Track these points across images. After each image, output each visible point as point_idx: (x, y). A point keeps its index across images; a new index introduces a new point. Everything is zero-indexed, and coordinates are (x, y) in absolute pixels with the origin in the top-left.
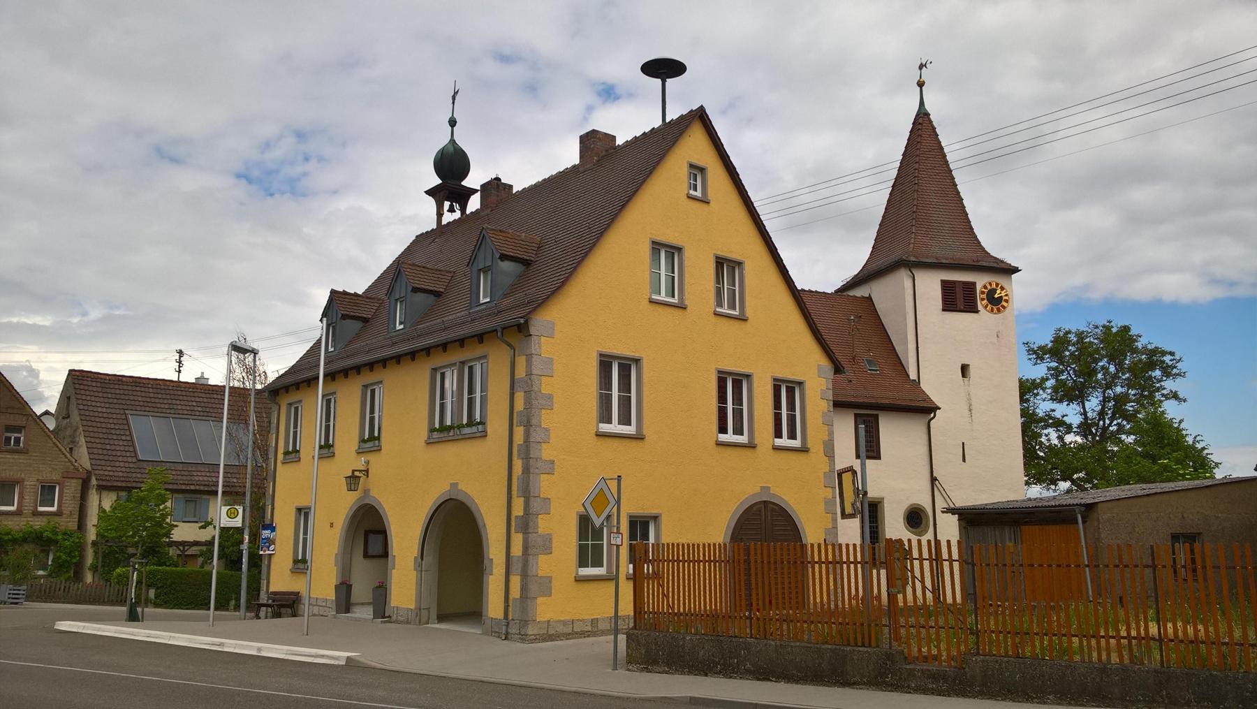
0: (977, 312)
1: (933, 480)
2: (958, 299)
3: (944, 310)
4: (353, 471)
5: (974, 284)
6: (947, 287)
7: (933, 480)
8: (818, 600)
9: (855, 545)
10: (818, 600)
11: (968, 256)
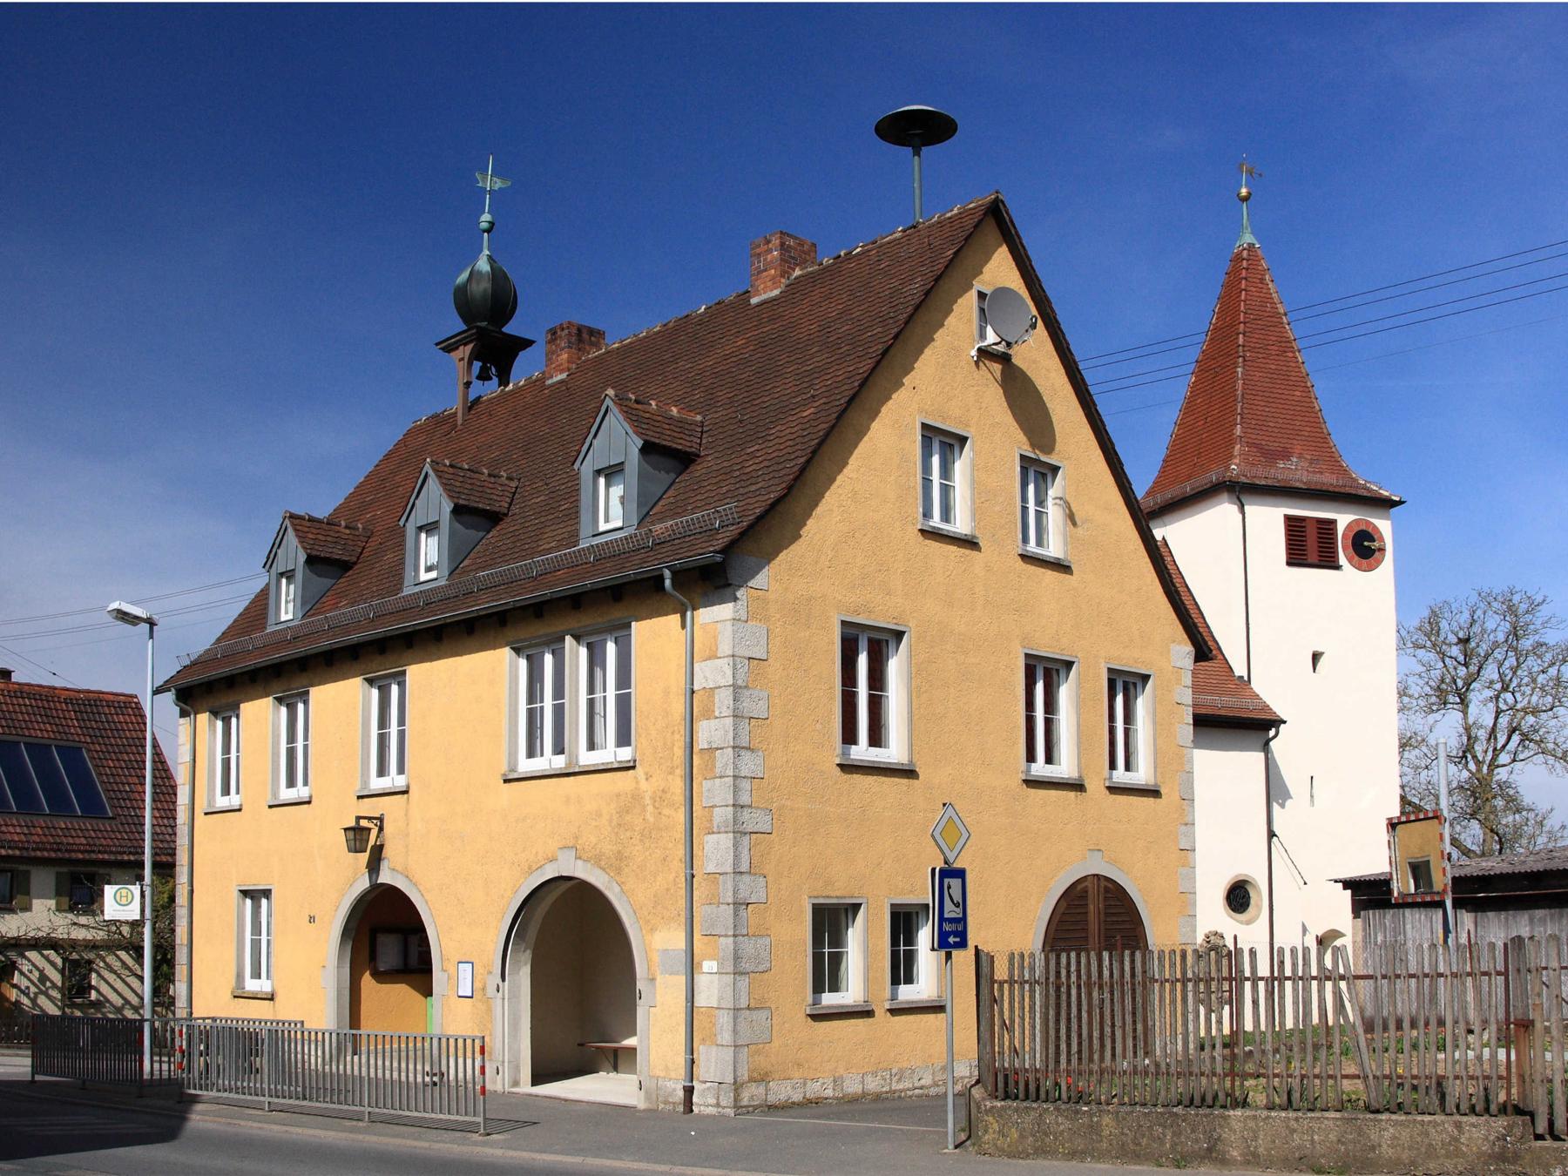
0: (1338, 567)
1: (1271, 834)
2: (1309, 547)
3: (1289, 564)
4: (358, 818)
5: (1333, 522)
6: (1294, 527)
7: (1271, 834)
8: (461, 1075)
9: (1032, 955)
10: (461, 1075)
11: (1328, 480)
